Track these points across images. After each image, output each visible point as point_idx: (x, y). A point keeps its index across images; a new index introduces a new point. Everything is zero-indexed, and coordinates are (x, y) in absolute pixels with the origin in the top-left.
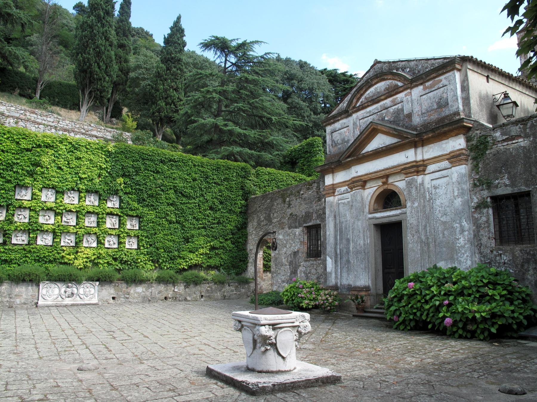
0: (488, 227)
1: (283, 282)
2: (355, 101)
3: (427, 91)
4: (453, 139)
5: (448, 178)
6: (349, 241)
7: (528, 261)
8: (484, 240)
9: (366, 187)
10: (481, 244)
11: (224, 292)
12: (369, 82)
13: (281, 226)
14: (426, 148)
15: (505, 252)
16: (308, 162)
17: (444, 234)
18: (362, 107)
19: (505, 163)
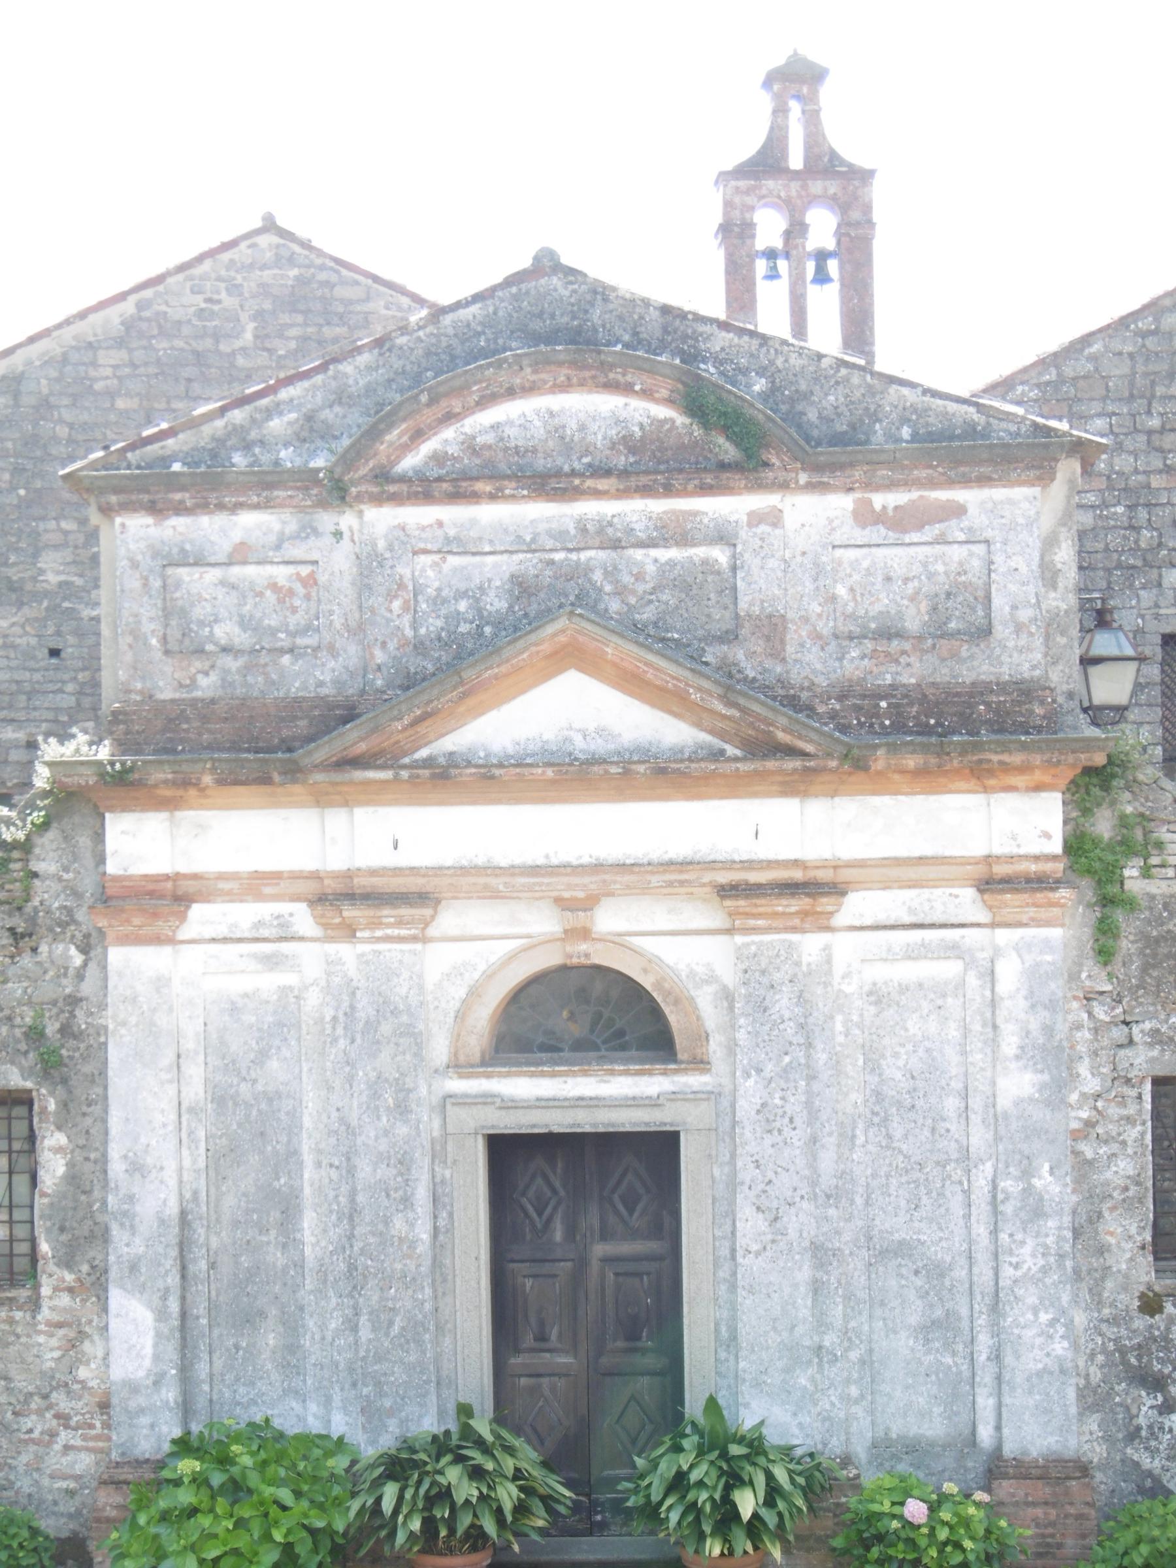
18: (452, 484)
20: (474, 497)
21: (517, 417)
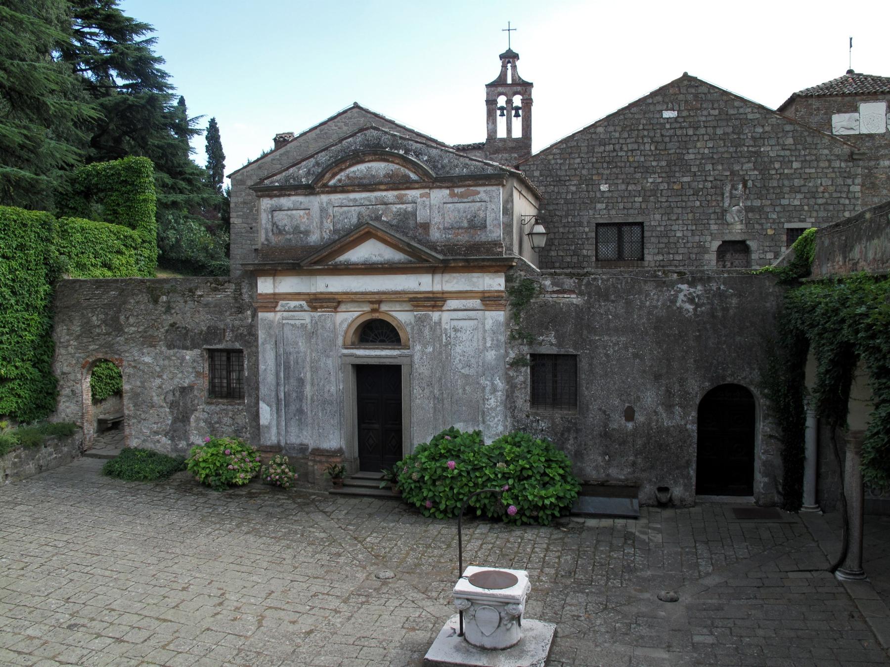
0: (525, 388)
1: (156, 433)
2: (328, 175)
3: (456, 199)
4: (490, 275)
5: (476, 322)
6: (303, 383)
7: (569, 430)
8: (520, 403)
9: (339, 310)
10: (515, 407)
11: (39, 460)
12: (358, 156)
13: (148, 341)
14: (447, 277)
15: (543, 418)
16: (128, 200)
17: (464, 390)
18: (341, 189)
19: (553, 318)
20: (348, 192)
21: (360, 169)
